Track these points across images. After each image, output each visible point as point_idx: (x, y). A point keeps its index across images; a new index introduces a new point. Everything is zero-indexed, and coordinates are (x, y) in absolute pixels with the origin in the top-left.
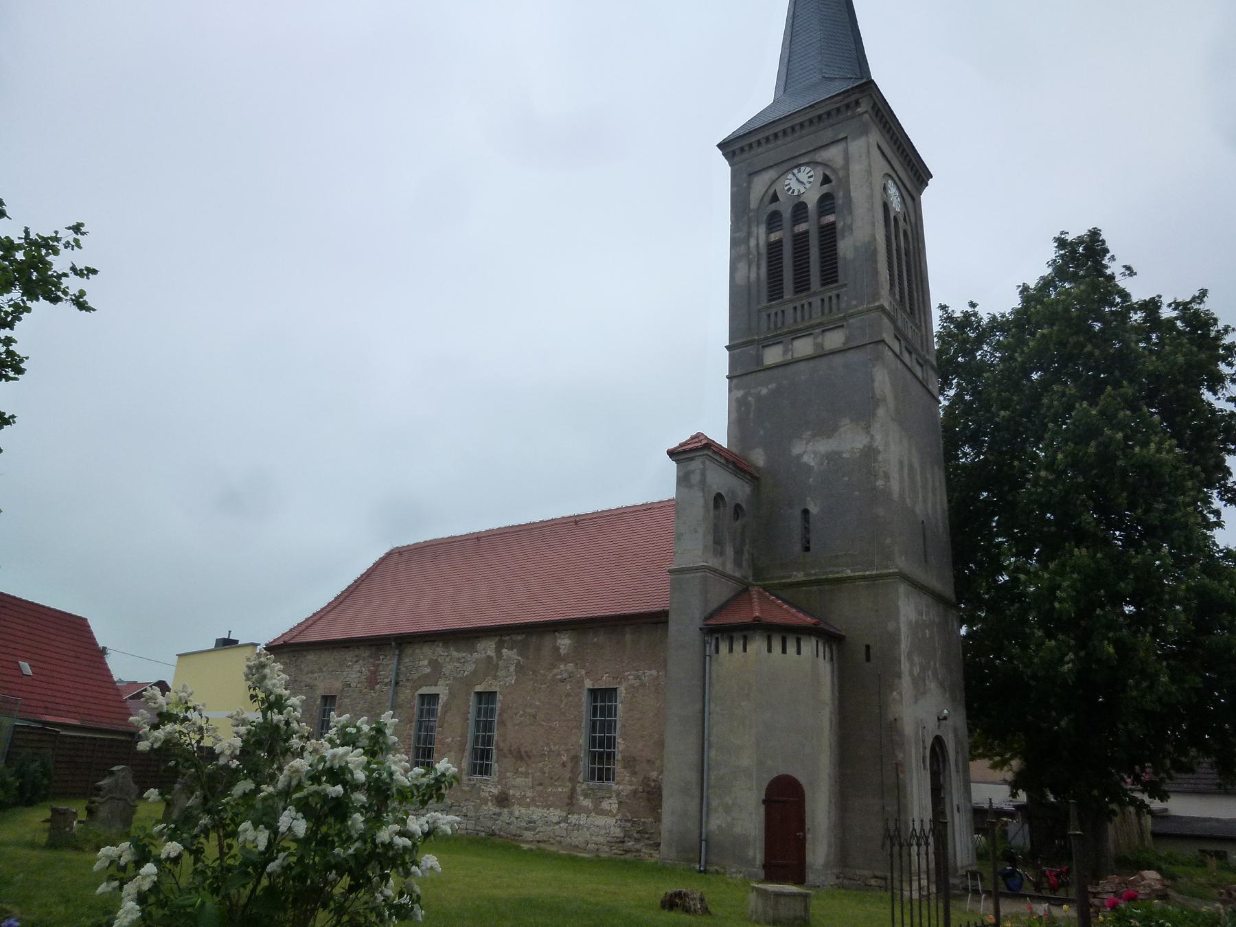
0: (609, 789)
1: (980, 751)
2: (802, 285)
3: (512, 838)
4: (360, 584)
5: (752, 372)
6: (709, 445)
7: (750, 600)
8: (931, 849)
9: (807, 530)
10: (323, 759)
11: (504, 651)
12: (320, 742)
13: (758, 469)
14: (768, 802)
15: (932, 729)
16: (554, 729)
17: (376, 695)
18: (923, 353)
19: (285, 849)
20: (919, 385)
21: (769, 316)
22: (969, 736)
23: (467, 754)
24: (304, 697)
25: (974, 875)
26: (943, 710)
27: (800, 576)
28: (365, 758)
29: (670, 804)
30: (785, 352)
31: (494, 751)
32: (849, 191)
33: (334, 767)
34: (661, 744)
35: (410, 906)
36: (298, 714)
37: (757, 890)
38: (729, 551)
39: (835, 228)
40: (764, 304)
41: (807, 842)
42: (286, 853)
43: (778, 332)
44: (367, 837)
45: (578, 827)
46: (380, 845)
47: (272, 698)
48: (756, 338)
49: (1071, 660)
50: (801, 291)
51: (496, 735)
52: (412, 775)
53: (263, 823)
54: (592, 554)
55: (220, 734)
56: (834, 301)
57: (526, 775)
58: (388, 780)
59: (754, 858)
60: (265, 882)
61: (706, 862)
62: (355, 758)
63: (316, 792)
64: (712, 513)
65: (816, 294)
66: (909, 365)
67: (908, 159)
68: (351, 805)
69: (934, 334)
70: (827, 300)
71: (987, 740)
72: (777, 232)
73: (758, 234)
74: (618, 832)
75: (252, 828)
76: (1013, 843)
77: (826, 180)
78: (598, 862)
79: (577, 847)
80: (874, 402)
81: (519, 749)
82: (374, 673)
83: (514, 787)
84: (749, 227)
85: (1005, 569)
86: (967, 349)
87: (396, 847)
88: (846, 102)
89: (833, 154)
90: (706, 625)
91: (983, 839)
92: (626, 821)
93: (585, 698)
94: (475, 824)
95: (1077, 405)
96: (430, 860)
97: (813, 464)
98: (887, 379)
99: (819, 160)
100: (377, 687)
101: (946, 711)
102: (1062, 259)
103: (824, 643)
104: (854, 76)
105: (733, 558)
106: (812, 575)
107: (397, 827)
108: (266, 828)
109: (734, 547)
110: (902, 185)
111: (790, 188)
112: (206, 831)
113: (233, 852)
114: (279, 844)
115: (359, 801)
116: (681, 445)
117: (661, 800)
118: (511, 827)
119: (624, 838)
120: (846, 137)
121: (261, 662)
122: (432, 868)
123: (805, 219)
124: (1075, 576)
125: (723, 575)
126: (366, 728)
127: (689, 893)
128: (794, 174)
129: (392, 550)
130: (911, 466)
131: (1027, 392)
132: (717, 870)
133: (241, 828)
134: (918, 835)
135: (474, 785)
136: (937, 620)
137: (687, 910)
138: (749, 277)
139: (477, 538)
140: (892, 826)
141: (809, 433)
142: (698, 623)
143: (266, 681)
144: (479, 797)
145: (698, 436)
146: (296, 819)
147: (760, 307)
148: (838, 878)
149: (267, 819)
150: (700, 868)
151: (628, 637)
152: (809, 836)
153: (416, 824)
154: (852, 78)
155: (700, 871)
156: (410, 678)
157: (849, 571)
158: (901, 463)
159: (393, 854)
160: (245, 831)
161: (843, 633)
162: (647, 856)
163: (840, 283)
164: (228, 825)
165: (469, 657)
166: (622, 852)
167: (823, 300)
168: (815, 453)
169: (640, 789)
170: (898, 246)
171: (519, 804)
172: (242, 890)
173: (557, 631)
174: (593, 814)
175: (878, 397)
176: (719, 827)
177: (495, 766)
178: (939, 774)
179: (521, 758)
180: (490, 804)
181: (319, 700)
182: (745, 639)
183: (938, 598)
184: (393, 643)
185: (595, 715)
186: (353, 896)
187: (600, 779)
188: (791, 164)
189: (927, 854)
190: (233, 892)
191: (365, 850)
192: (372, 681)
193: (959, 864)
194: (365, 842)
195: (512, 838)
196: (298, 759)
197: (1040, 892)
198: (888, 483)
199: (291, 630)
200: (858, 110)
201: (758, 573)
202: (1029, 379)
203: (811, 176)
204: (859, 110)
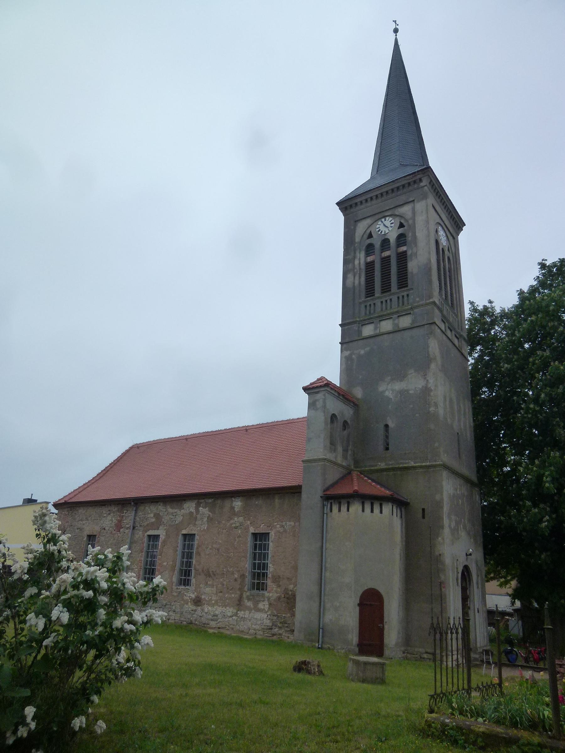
0: (263, 595)
1: (492, 575)
2: (386, 288)
3: (203, 625)
4: (113, 466)
5: (402, 330)
6: (328, 384)
7: (352, 480)
8: (460, 635)
9: (387, 437)
10: (81, 574)
11: (201, 508)
12: (79, 563)
13: (358, 399)
14: (361, 605)
15: (462, 561)
16: (230, 558)
17: (121, 535)
18: (459, 331)
19: (55, 631)
20: (456, 351)
21: (366, 306)
22: (485, 566)
23: (176, 572)
24: (70, 535)
25: (487, 652)
26: (469, 549)
27: (382, 465)
28: (107, 574)
29: (300, 605)
30: (376, 328)
31: (193, 571)
32: (415, 232)
33: (88, 579)
34: (295, 568)
35: (133, 668)
36: (66, 546)
37: (354, 660)
38: (340, 449)
39: (406, 254)
40: (363, 299)
41: (385, 630)
42: (56, 634)
43: (372, 316)
44: (107, 624)
45: (243, 619)
46: (115, 629)
47: (50, 535)
48: (358, 320)
49: (547, 521)
50: (385, 292)
51: (194, 561)
52: (138, 585)
53: (42, 614)
54: (228, 453)
55: (16, 558)
56: (406, 298)
57: (212, 586)
58: (122, 588)
59: (352, 640)
60: (43, 652)
61: (322, 643)
62: (102, 574)
63: (75, 595)
64: (329, 426)
65: (394, 294)
66: (450, 338)
67: (451, 214)
68: (98, 604)
69: (466, 319)
70: (401, 298)
71: (497, 568)
72: (371, 256)
73: (360, 257)
74: (268, 623)
75: (34, 617)
76: (512, 632)
77: (401, 226)
78: (255, 642)
79: (243, 631)
80: (429, 360)
81: (208, 569)
82: (120, 521)
83: (205, 593)
84: (355, 253)
85: (508, 462)
86: (485, 328)
87: (126, 631)
88: (414, 179)
89: (406, 210)
90: (324, 494)
91: (494, 630)
92: (273, 616)
93: (250, 538)
94: (180, 617)
95: (552, 364)
96: (147, 639)
97: (391, 397)
98: (437, 345)
99: (397, 214)
100: (121, 530)
101: (471, 550)
102: (543, 276)
103: (397, 507)
104: (419, 164)
105: (341, 454)
106: (390, 465)
107: (126, 618)
108: (44, 617)
109: (342, 447)
110: (446, 229)
111: (380, 230)
112: (7, 619)
113: (24, 633)
114: (52, 627)
115: (103, 601)
116: (311, 384)
117: (295, 603)
118: (202, 618)
119: (272, 626)
120: (414, 201)
121: (43, 513)
122: (148, 644)
123: (389, 248)
124: (552, 468)
125: (335, 463)
126: (110, 556)
127: (311, 661)
128: (382, 222)
129: (133, 445)
130: (451, 400)
131: (522, 355)
132: (329, 647)
133: (27, 618)
134: (452, 627)
135: (180, 592)
136: (466, 493)
137: (309, 672)
138: (354, 283)
139: (186, 439)
140: (435, 621)
141: (389, 378)
142: (320, 493)
143: (46, 525)
144: (183, 600)
145: (322, 379)
146: (62, 612)
147: (361, 301)
148: (404, 653)
149: (45, 612)
150: (319, 645)
151: (277, 501)
152: (386, 627)
153: (138, 616)
154: (418, 165)
155: (319, 648)
156: (142, 525)
157: (413, 463)
158: (445, 398)
159: (124, 635)
160: (30, 619)
161: (409, 501)
162: (286, 638)
163: (409, 287)
164: (22, 615)
165: (179, 512)
166: (270, 635)
167: (398, 298)
168: (393, 390)
169: (283, 596)
170: (444, 266)
171: (208, 604)
172: (28, 656)
173: (233, 497)
174: (253, 611)
175: (431, 357)
176: (331, 620)
177: (193, 581)
178: (467, 589)
179: (210, 576)
180: (189, 604)
181: (86, 538)
182: (349, 504)
183: (467, 480)
184: (132, 503)
185: (255, 549)
186: (98, 661)
187: (258, 589)
188: (380, 215)
189: (457, 639)
190: (23, 657)
191: (106, 632)
192: (119, 527)
193: (478, 645)
194: (106, 627)
195: (203, 625)
196: (65, 574)
197: (528, 663)
198: (437, 409)
199: (69, 494)
200: (421, 184)
201: (357, 462)
202: (523, 347)
203: (392, 223)
204: (422, 184)
